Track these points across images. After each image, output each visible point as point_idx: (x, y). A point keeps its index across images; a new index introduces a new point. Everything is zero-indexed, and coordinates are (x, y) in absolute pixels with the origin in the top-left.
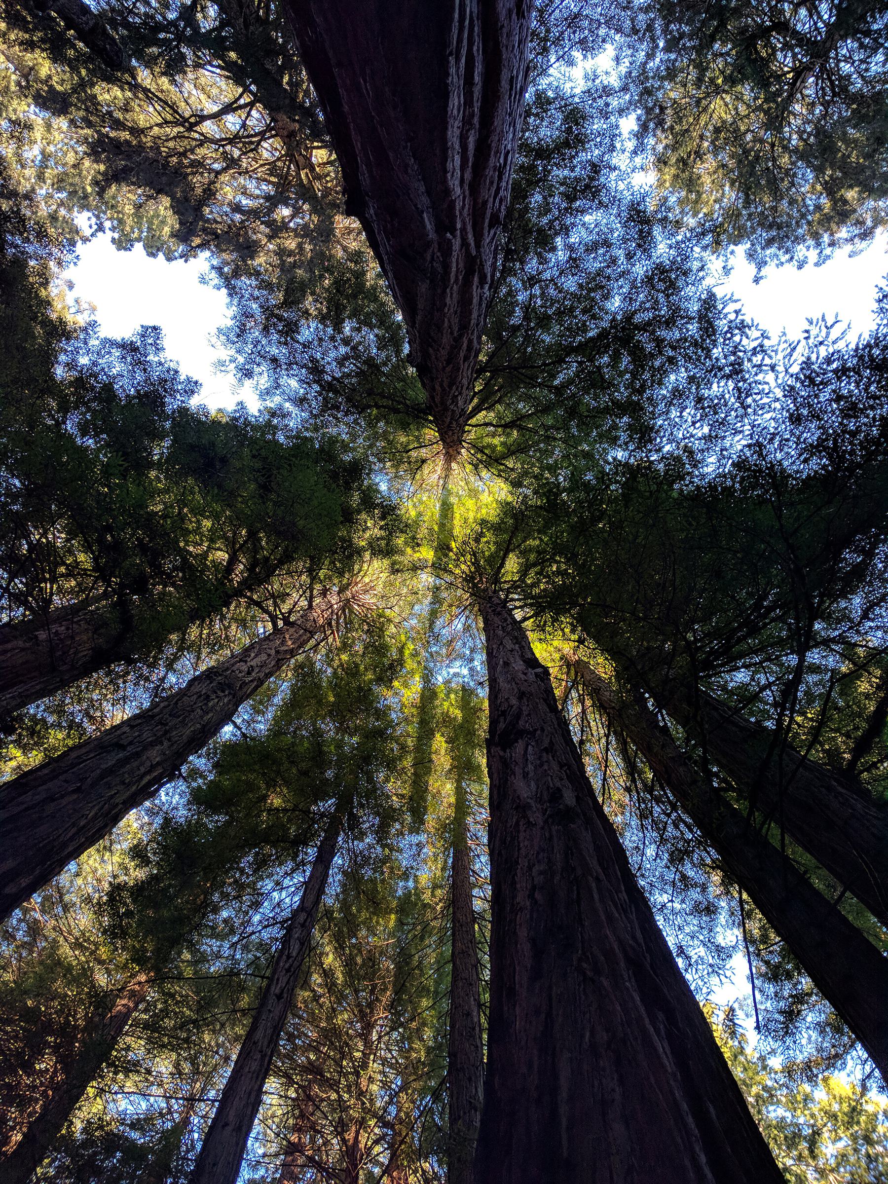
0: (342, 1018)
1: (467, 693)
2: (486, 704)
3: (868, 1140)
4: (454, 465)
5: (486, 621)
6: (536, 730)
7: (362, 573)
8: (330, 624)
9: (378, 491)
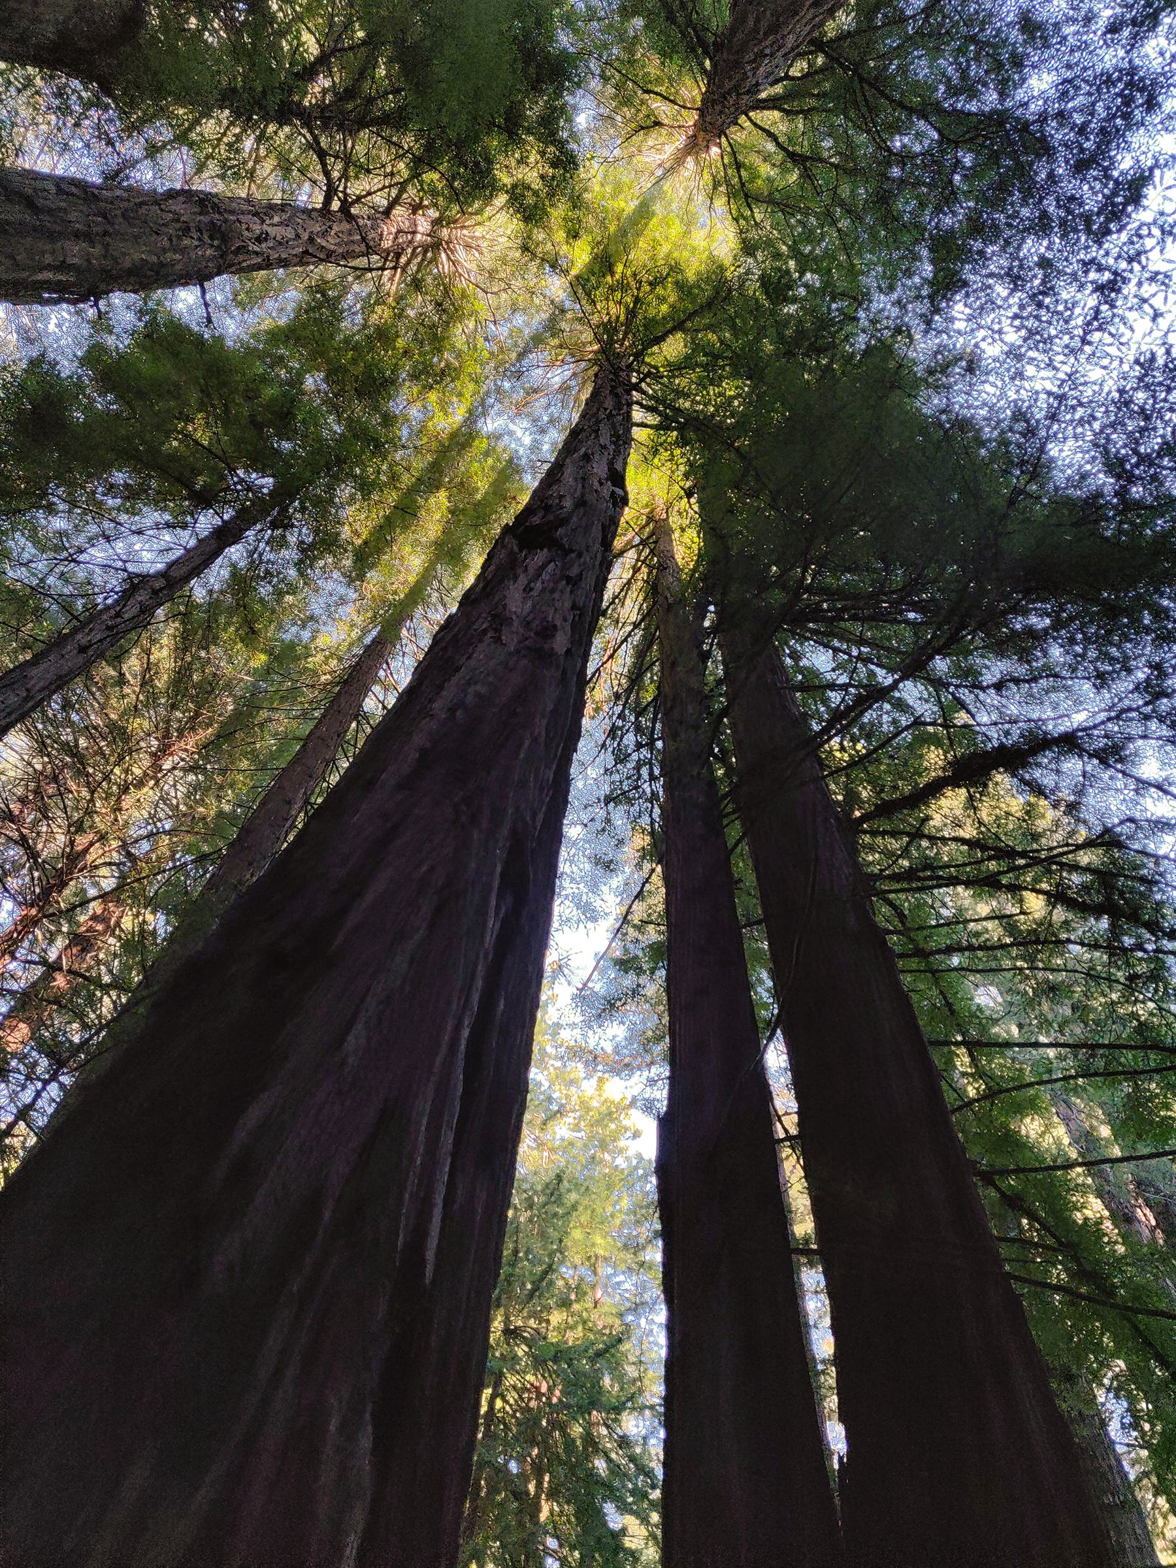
0: (138, 725)
1: (510, 470)
2: (525, 499)
3: (603, 1145)
4: (690, 162)
5: (594, 395)
6: (573, 551)
7: (478, 218)
8: (398, 256)
9: (569, 120)
